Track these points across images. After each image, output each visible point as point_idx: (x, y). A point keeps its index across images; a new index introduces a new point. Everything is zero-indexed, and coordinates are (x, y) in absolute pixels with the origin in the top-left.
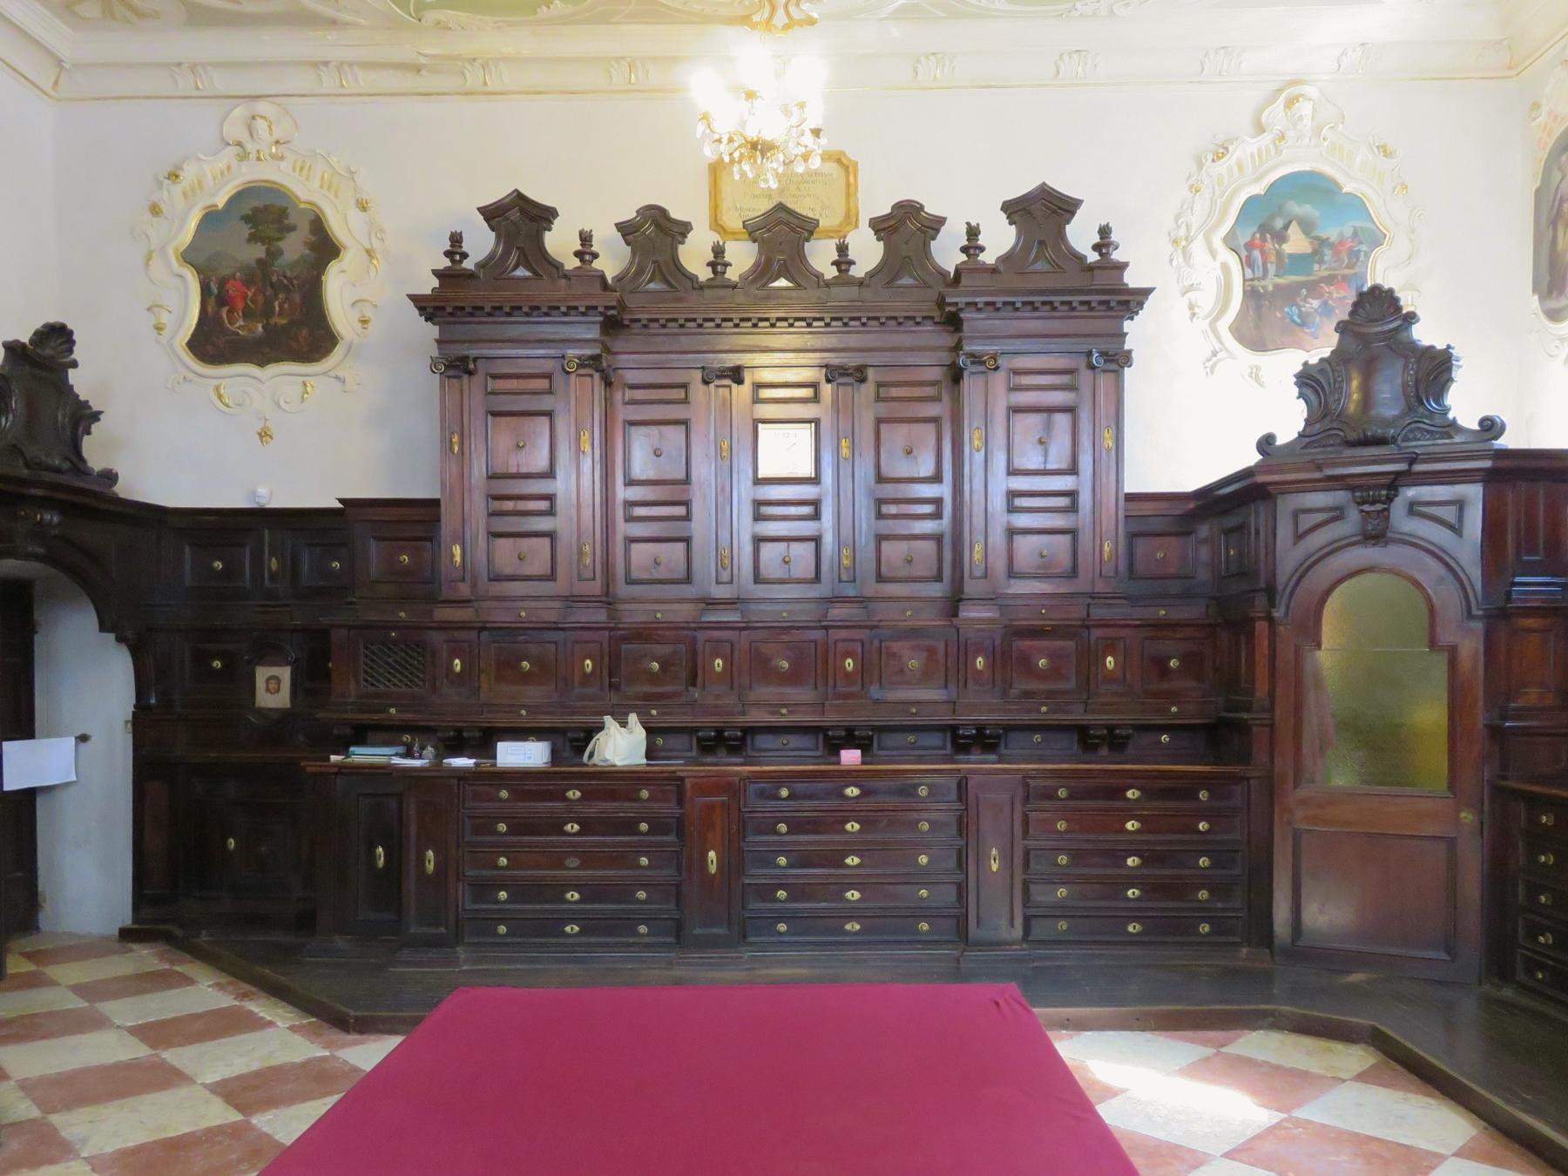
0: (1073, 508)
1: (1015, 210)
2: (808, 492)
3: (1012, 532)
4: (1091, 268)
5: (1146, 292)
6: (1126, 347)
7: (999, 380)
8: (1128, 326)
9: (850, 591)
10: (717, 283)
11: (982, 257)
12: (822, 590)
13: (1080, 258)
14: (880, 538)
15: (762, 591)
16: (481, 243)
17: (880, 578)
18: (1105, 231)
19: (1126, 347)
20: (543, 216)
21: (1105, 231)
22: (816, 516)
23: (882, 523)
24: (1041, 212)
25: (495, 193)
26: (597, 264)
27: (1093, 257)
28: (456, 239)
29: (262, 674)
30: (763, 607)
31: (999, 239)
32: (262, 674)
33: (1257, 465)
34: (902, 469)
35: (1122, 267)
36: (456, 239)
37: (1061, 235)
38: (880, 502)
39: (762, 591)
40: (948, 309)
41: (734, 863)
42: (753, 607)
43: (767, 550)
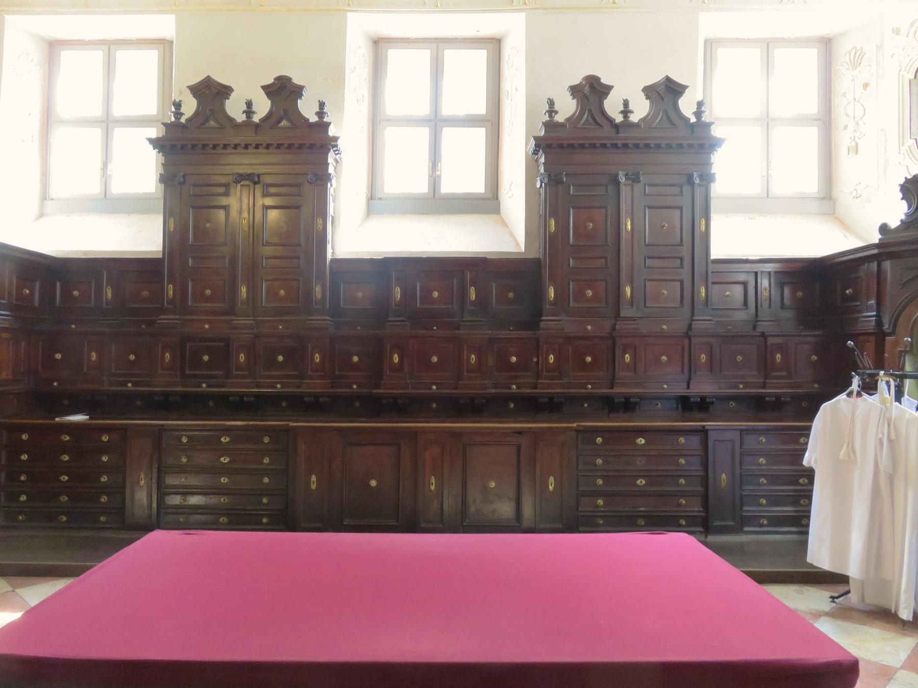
20: (224, 91)
25: (655, 78)
31: (263, 106)
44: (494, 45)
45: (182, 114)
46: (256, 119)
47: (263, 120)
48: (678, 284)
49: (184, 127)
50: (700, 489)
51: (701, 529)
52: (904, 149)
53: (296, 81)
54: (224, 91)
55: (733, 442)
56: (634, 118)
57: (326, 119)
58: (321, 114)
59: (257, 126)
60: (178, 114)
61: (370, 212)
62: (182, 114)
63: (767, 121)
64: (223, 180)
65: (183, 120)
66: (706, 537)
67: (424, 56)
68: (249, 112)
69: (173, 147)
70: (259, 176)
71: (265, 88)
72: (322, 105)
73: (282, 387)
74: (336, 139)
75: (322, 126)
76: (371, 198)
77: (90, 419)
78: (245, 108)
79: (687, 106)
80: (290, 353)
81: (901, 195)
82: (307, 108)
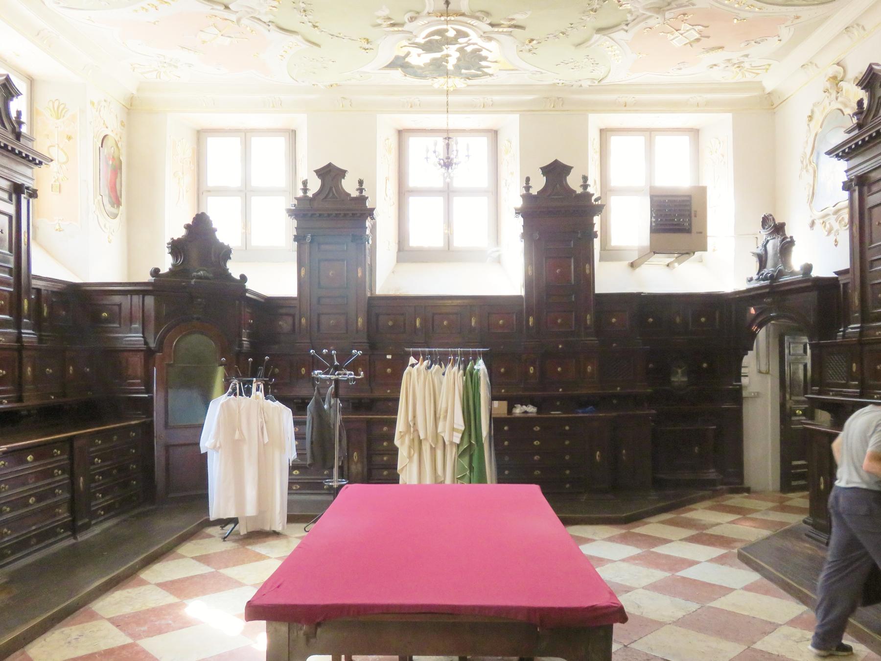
20: (342, 173)
44: (293, 134)
46: (310, 194)
47: (315, 195)
49: (311, 200)
51: (69, 533)
52: (96, 201)
54: (342, 173)
55: (791, 394)
57: (364, 193)
58: (361, 190)
60: (305, 190)
61: (399, 260)
63: (448, 192)
66: (75, 538)
67: (235, 142)
69: (305, 215)
71: (317, 172)
72: (361, 182)
74: (373, 210)
75: (362, 199)
76: (400, 250)
77: (538, 412)
81: (175, 238)
82: (349, 186)
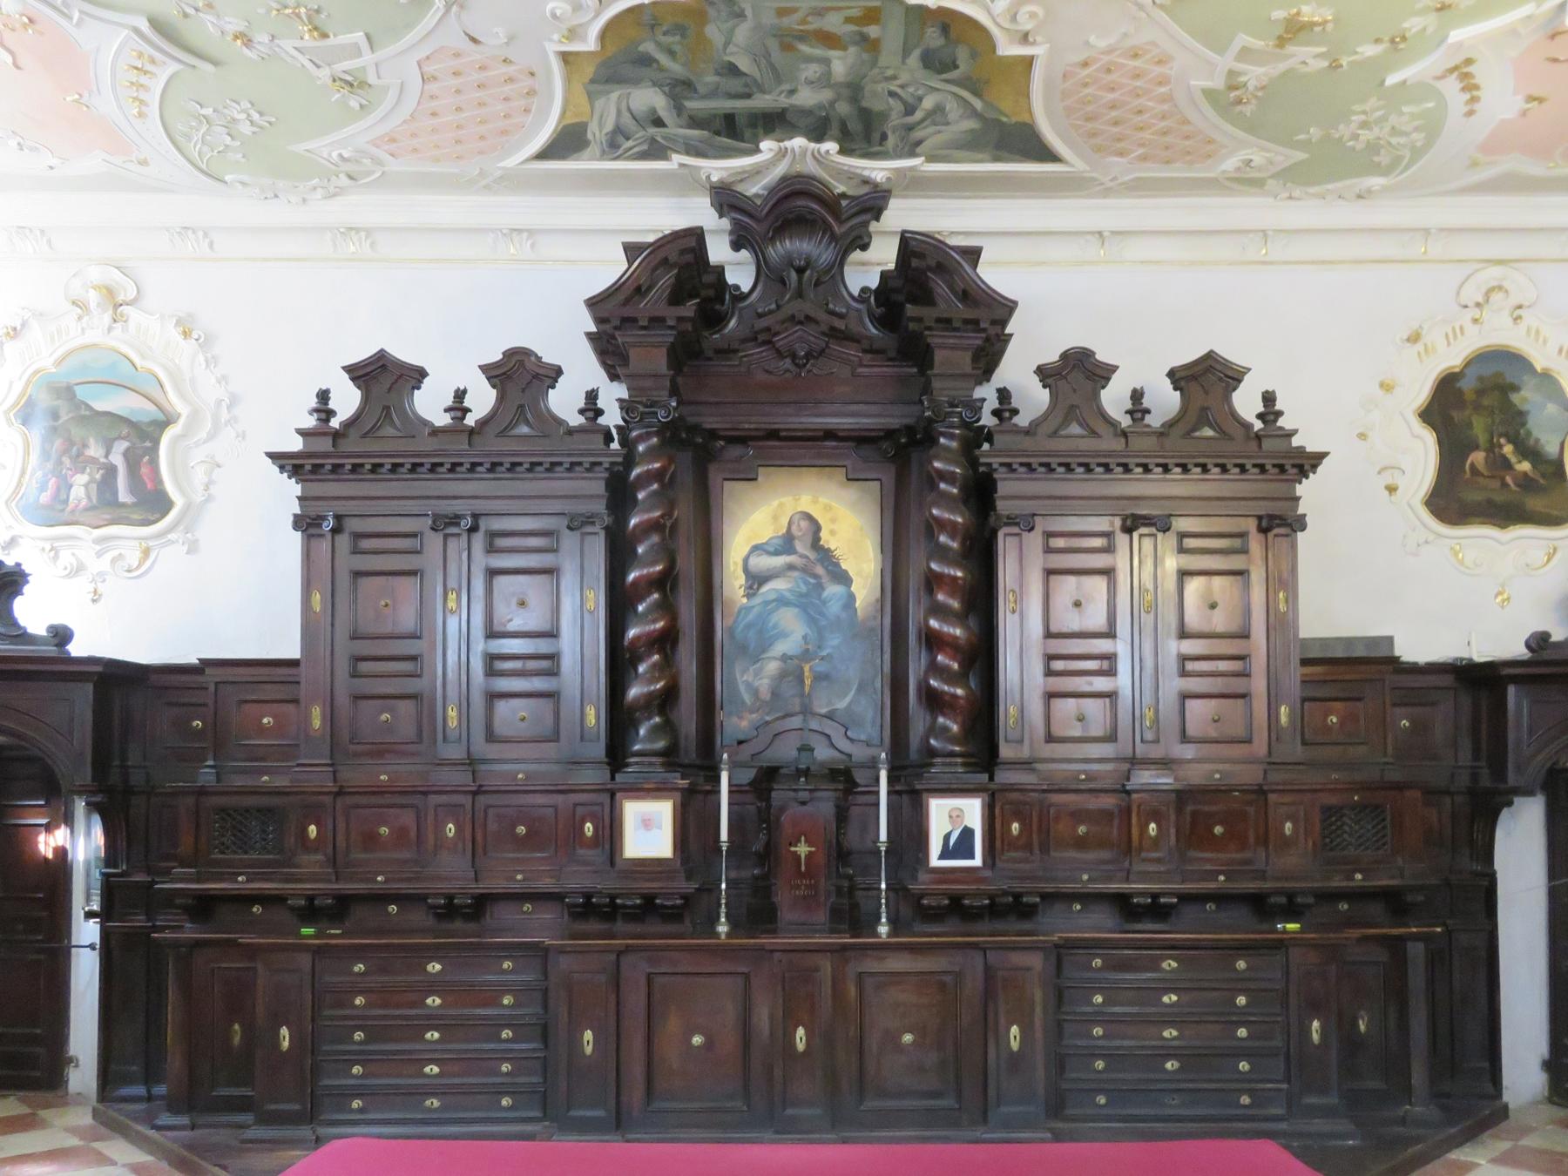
0: (553, 673)
1: (1179, 377)
2: (542, 646)
3: (493, 697)
4: (1258, 437)
5: (1320, 457)
6: (1300, 511)
7: (1034, 541)
8: (1300, 489)
9: (1156, 752)
10: (389, 442)
11: (1148, 419)
12: (1123, 747)
13: (1248, 426)
14: (1050, 696)
15: (493, 751)
16: (347, 400)
17: (1050, 738)
18: (1269, 398)
19: (1300, 511)
20: (1100, 374)
21: (1269, 398)
22: (1111, 672)
23: (1051, 679)
24: (1206, 379)
25: (361, 352)
26: (601, 420)
27: (1258, 425)
28: (324, 396)
29: (633, 810)
30: (497, 767)
31: (1165, 401)
32: (633, 810)
33: (42, 637)
34: (1072, 622)
35: (1290, 434)
36: (324, 396)
37: (1227, 398)
38: (1050, 658)
39: (493, 751)
40: (982, 469)
41: (308, 1043)
42: (483, 767)
43: (502, 707)
45: (467, 410)
47: (483, 423)
48: (1191, 705)
49: (337, 435)
50: (1486, 1065)
53: (1102, 356)
54: (1100, 374)
56: (1154, 421)
59: (471, 432)
62: (467, 410)
64: (1102, 524)
65: (335, 423)
68: (458, 407)
70: (476, 516)
73: (248, 881)
78: (313, 402)
79: (1246, 402)
80: (1233, 819)
